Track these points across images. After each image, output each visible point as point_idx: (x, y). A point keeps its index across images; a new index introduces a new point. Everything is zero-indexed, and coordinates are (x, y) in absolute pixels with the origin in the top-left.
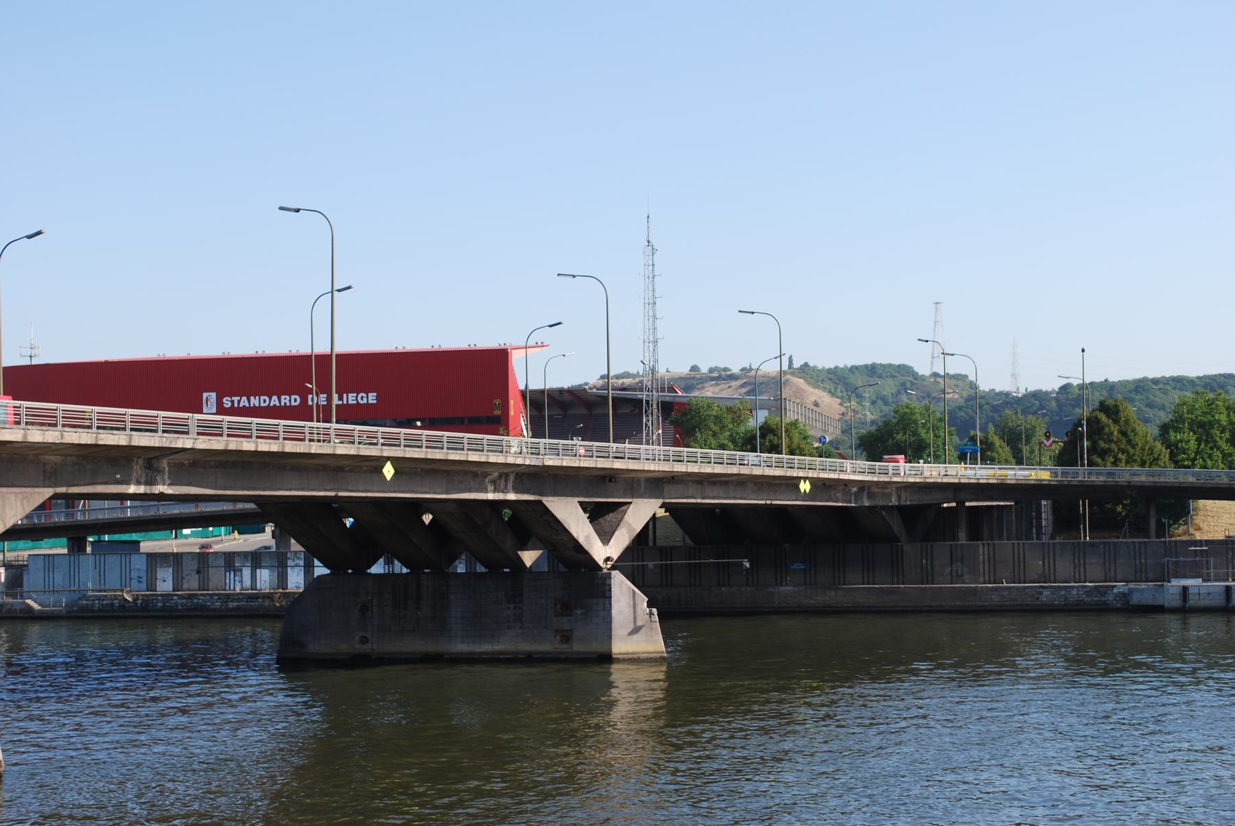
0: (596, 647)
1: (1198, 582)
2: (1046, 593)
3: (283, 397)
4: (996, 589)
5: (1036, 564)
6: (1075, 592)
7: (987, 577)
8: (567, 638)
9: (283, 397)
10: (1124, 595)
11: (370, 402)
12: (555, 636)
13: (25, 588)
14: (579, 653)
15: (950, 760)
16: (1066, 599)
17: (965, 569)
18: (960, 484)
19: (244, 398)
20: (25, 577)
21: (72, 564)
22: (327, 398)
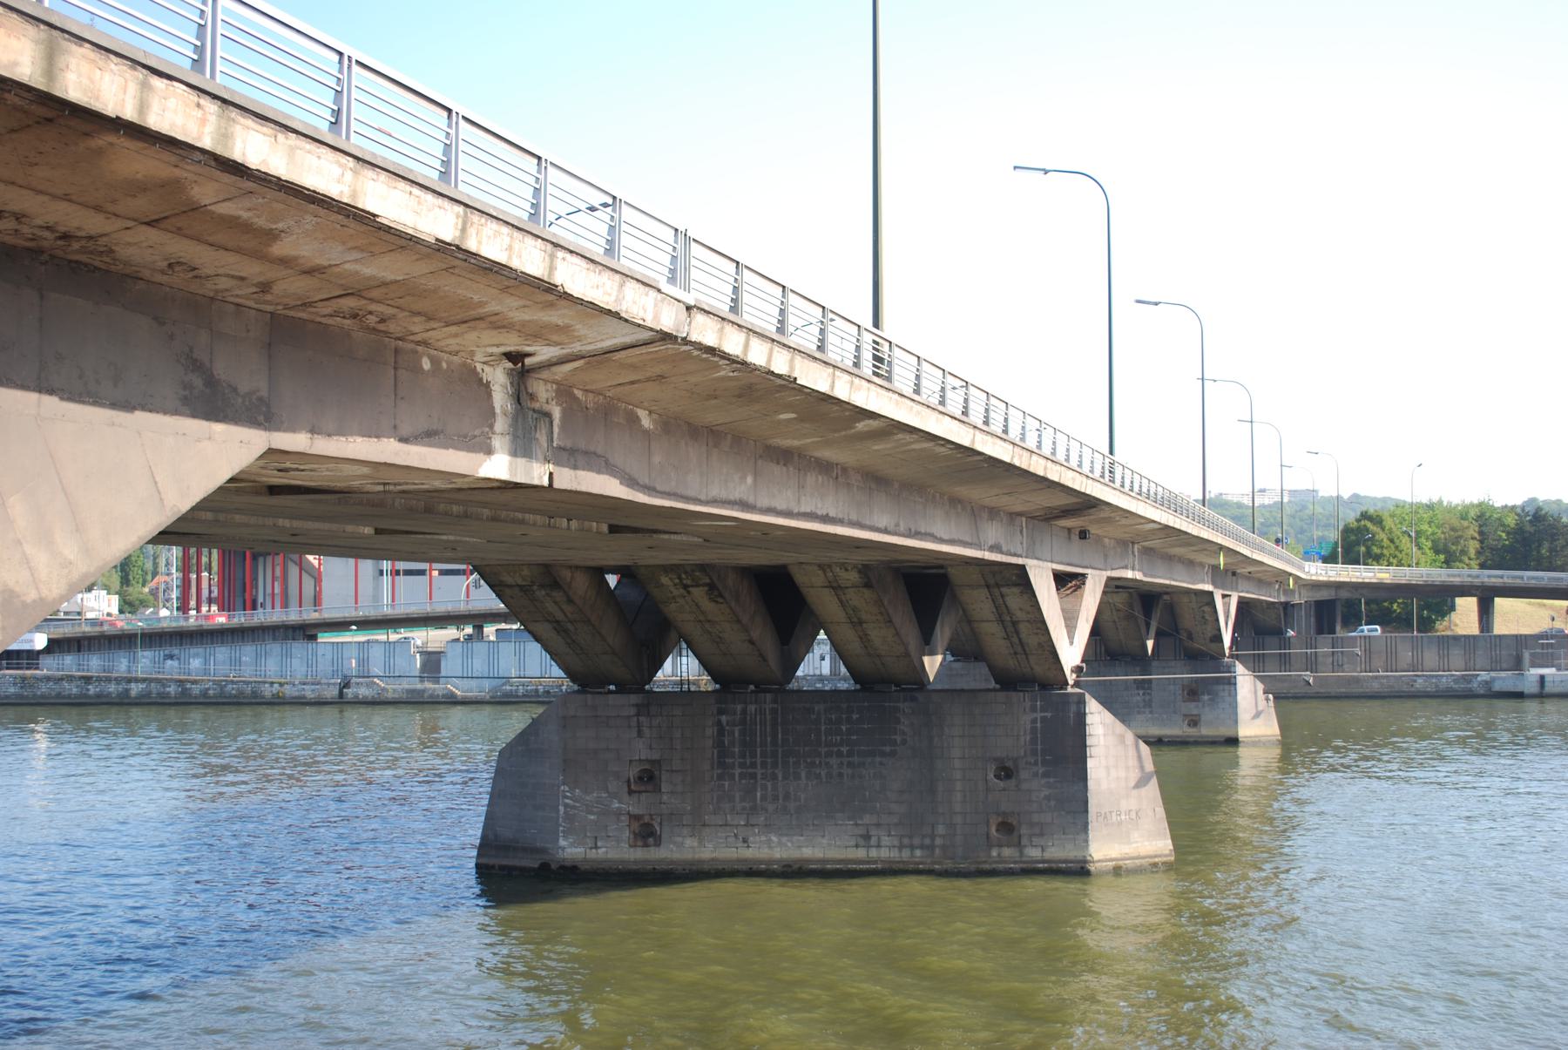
0: (1224, 731)
1: (1552, 671)
2: (1420, 681)
4: (1376, 677)
5: (1406, 655)
6: (1444, 680)
7: (1363, 666)
8: (1194, 722)
10: (1487, 682)
12: (1183, 721)
13: (443, 673)
14: (1208, 737)
16: (1437, 686)
17: (1345, 659)
18: (1363, 583)
20: (443, 664)
21: (491, 650)
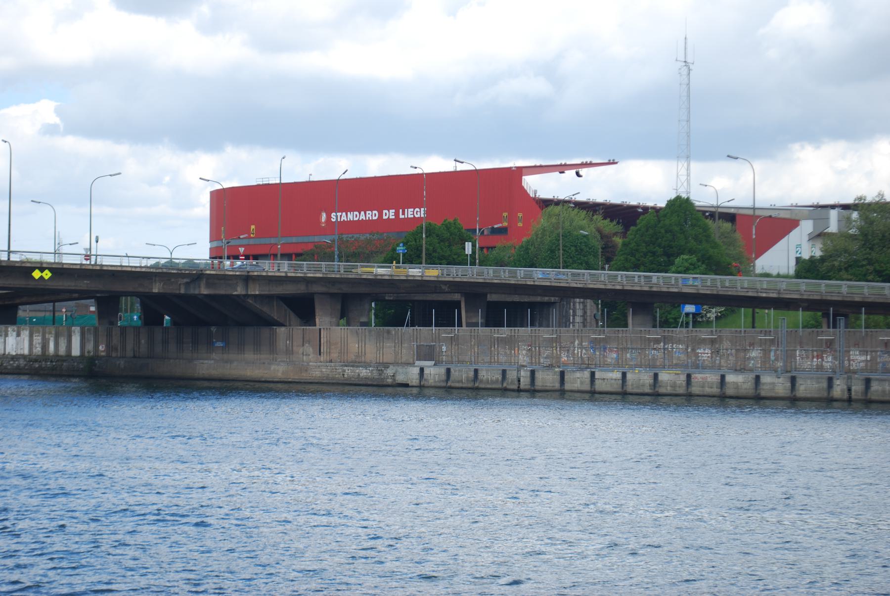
3: (368, 212)
9: (368, 212)
11: (391, 217)
15: (98, 547)
19: (344, 214)
22: (395, 213)
